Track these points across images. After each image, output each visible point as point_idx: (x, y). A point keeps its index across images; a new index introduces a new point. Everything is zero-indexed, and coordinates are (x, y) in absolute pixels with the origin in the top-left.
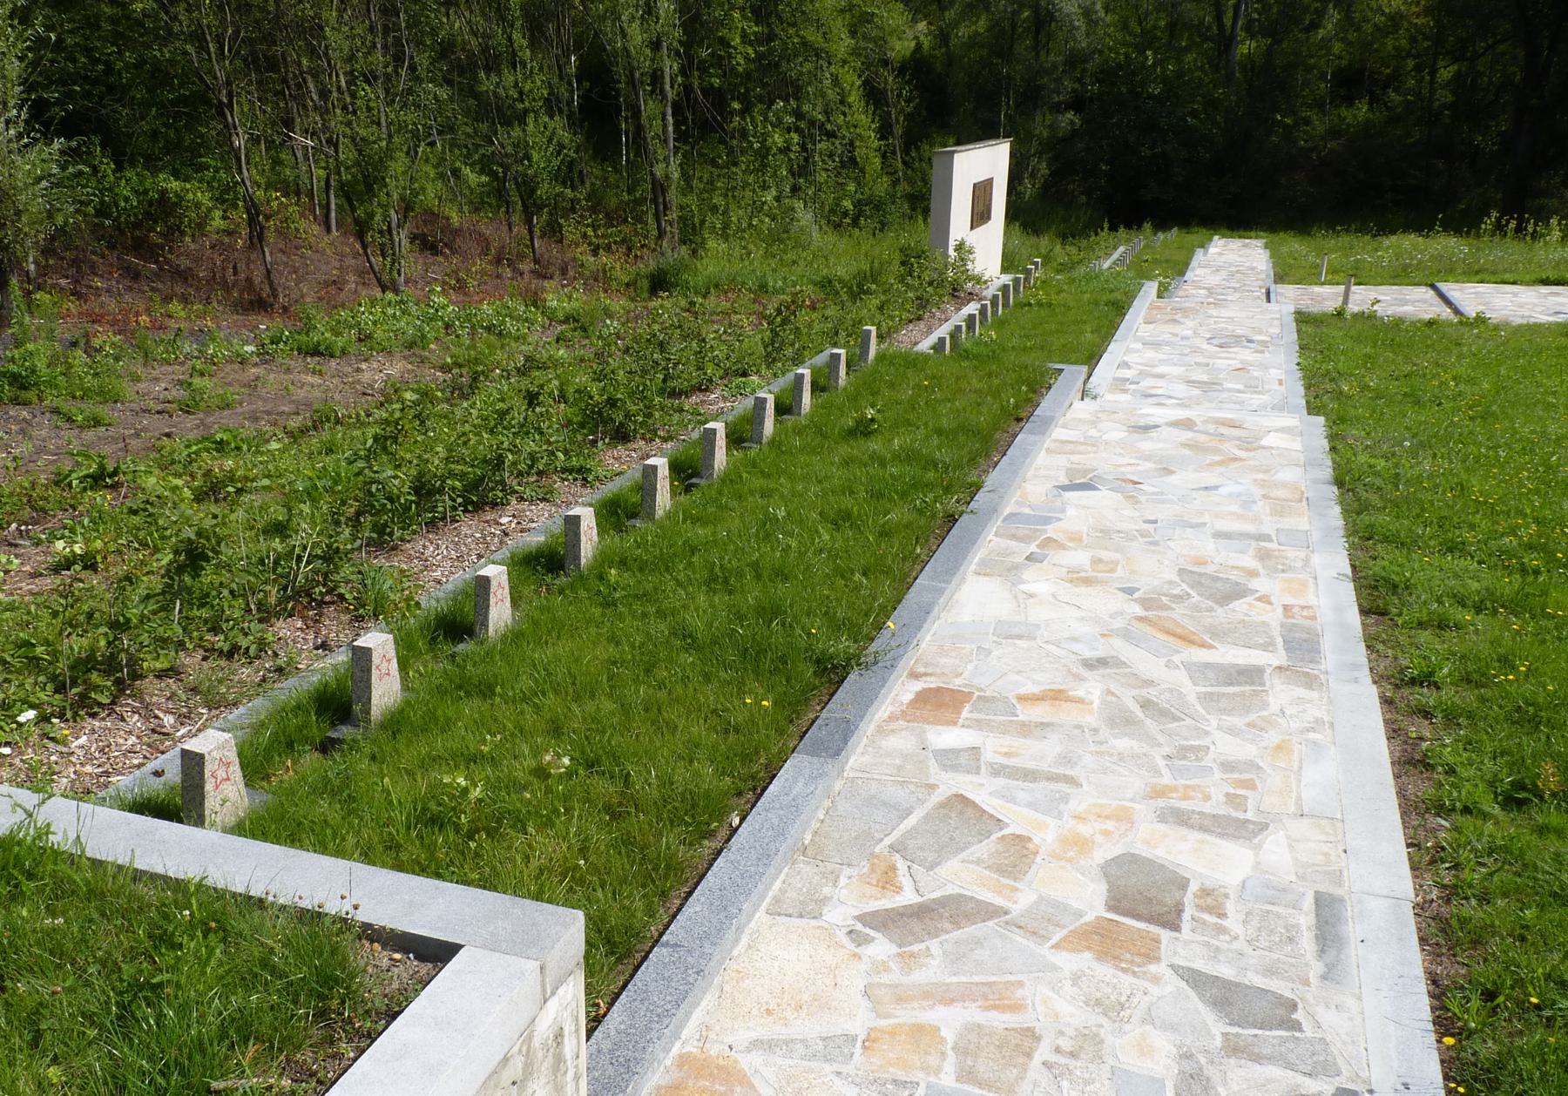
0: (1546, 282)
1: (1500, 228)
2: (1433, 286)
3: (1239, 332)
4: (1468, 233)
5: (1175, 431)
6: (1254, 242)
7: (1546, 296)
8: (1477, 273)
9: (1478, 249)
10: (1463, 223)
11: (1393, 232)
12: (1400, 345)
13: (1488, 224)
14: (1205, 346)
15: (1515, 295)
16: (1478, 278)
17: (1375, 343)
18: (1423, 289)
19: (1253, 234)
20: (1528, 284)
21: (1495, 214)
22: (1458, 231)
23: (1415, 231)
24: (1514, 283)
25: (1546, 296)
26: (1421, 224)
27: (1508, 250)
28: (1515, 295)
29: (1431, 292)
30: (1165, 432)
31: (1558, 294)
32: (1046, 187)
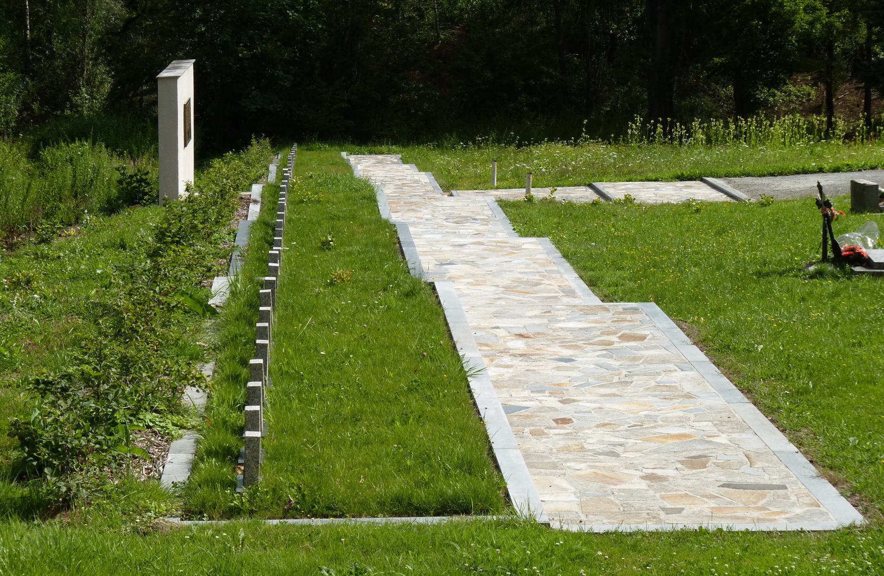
0: (681, 178)
1: (647, 135)
2: (591, 186)
3: (463, 214)
4: (616, 140)
5: (477, 246)
6: (389, 158)
7: (681, 189)
8: (629, 173)
9: (627, 156)
10: (610, 130)
11: (538, 141)
12: (576, 217)
13: (634, 128)
14: (445, 223)
15: (657, 189)
16: (628, 177)
17: (560, 217)
18: (583, 188)
19: (384, 148)
20: (667, 180)
21: (639, 119)
22: (606, 138)
23: (562, 139)
24: (656, 180)
25: (681, 189)
26: (567, 133)
27: (658, 154)
28: (657, 189)
29: (590, 191)
30: (472, 246)
31: (691, 187)
32: (114, 96)
